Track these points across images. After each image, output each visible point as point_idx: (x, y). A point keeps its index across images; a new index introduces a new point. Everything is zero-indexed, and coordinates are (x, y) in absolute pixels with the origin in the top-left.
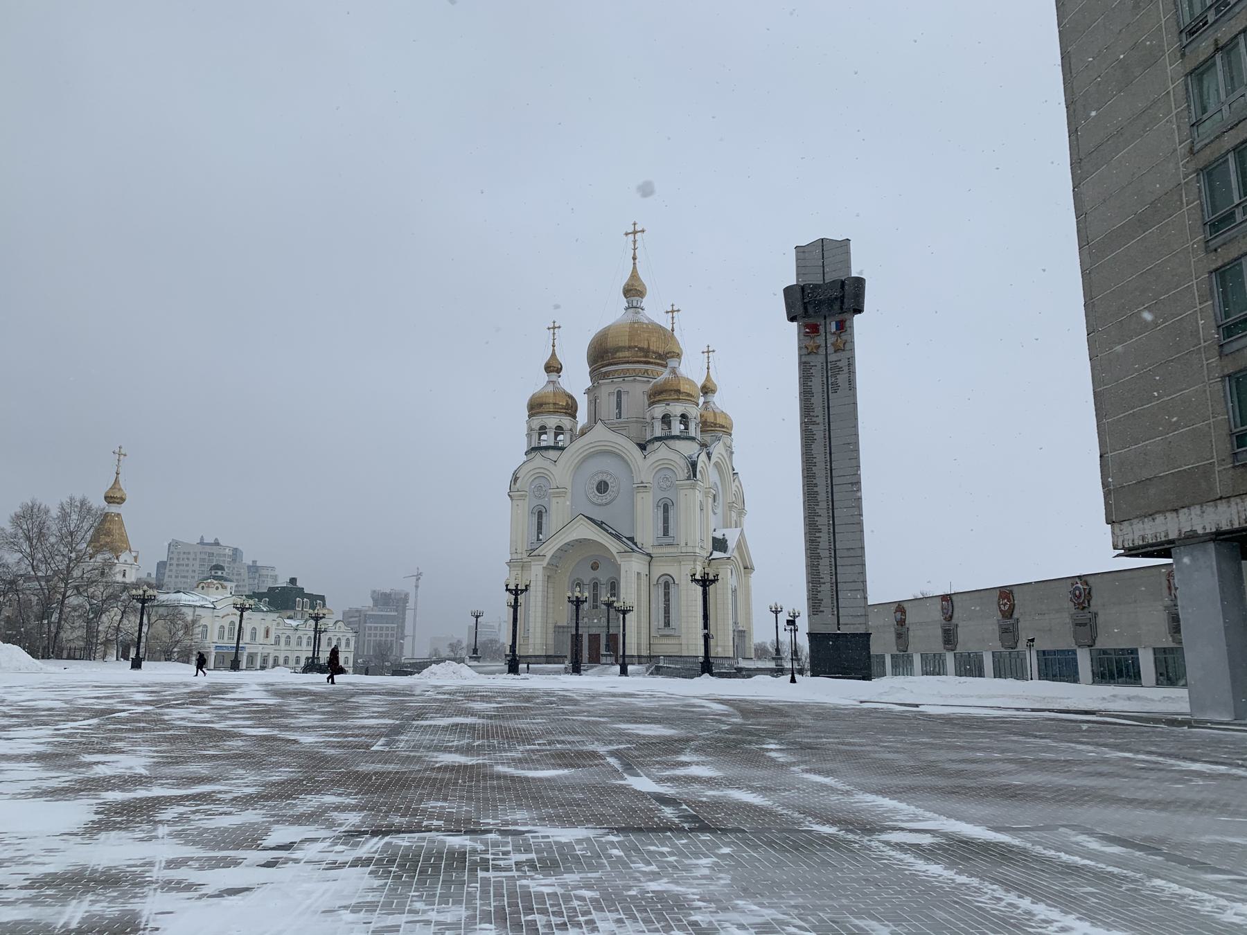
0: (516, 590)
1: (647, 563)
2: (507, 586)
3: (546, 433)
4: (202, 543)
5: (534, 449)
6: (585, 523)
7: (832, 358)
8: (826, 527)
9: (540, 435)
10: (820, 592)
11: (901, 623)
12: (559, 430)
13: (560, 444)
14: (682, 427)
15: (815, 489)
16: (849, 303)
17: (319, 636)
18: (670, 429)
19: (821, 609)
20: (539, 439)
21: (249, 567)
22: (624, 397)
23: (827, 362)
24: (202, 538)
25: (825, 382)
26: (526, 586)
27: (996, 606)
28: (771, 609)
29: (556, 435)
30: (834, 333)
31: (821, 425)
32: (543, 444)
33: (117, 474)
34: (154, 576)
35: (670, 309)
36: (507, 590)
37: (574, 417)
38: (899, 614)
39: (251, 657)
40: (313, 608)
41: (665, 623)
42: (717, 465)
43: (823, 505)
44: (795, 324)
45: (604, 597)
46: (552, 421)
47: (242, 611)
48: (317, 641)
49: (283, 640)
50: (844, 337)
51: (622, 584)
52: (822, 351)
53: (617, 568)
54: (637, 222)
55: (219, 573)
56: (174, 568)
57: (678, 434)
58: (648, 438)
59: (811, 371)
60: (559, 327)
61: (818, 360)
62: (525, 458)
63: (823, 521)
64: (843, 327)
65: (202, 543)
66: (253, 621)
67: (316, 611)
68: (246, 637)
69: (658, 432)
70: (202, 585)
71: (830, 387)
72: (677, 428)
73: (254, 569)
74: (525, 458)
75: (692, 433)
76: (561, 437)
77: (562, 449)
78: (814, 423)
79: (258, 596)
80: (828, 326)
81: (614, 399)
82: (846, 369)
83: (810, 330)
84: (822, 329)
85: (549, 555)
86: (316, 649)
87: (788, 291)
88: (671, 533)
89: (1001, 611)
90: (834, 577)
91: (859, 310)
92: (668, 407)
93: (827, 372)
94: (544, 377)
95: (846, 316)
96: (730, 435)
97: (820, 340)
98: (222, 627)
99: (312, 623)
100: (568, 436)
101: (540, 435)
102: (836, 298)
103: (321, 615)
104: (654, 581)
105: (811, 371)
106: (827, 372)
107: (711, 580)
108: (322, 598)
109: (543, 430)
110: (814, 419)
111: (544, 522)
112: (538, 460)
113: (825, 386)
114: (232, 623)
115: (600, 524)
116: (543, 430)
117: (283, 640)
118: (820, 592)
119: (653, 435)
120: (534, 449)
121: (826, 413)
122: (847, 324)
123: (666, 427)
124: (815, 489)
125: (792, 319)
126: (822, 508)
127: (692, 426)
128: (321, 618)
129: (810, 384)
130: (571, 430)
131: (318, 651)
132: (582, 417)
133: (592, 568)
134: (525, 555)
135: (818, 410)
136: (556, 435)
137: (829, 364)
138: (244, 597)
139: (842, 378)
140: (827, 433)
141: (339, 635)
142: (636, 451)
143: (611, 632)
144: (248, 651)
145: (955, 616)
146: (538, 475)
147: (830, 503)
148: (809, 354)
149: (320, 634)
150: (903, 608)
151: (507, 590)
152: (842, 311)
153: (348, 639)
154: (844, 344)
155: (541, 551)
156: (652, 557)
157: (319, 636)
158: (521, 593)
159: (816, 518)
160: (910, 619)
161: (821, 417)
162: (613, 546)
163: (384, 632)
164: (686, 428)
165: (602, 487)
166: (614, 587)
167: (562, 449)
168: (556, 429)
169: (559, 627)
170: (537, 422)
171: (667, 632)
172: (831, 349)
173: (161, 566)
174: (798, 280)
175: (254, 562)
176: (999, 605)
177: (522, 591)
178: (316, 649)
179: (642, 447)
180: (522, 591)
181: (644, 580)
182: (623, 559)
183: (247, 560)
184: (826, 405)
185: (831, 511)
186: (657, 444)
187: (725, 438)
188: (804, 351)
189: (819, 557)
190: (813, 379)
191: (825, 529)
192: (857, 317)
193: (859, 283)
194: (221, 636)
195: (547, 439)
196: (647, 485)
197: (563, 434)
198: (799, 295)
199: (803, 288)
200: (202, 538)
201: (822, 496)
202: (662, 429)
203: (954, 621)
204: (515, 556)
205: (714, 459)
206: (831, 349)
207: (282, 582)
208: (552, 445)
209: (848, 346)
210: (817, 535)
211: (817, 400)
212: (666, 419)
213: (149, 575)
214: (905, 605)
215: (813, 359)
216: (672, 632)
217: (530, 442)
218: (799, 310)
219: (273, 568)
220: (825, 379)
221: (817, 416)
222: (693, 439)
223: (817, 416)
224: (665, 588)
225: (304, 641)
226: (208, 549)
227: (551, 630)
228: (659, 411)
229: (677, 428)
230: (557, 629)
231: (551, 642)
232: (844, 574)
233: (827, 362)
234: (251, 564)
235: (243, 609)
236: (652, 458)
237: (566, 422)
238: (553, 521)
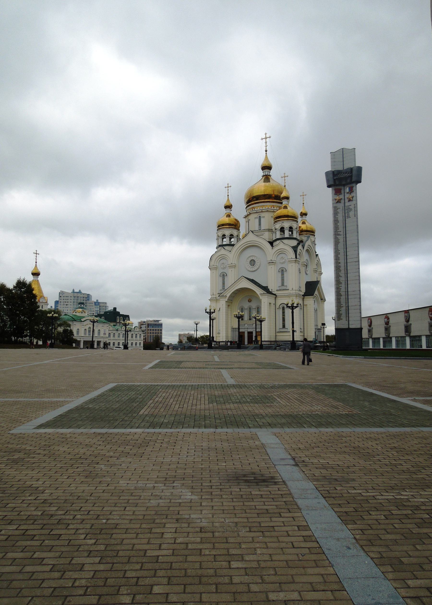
0: (210, 312)
1: (274, 299)
2: (206, 310)
3: (225, 238)
4: (73, 292)
5: (220, 246)
6: (244, 280)
7: (347, 204)
8: (344, 282)
9: (223, 239)
10: (341, 310)
11: (387, 323)
12: (231, 236)
13: (233, 243)
14: (291, 233)
15: (339, 265)
16: (354, 179)
17: (127, 333)
18: (284, 234)
19: (341, 318)
20: (223, 241)
21: (95, 303)
22: (262, 220)
23: (345, 206)
24: (73, 290)
25: (344, 215)
26: (214, 310)
27: (427, 315)
28: (333, 318)
29: (230, 239)
30: (348, 193)
31: (342, 235)
32: (224, 243)
33: (36, 262)
34: (53, 307)
35: (283, 176)
36: (206, 312)
37: (239, 230)
38: (386, 320)
39: (99, 343)
40: (124, 320)
41: (283, 326)
42: (307, 250)
43: (343, 272)
44: (331, 189)
45: (254, 314)
46: (227, 232)
47: (94, 323)
48: (126, 335)
49: (112, 335)
50: (353, 194)
51: (262, 309)
52: (342, 201)
53: (260, 301)
54: (267, 133)
55: (82, 306)
56: (62, 303)
57: (288, 236)
58: (274, 239)
59: (338, 211)
60: (231, 187)
61: (341, 205)
62: (216, 250)
63: (342, 279)
64: (351, 190)
65: (73, 292)
66: (98, 327)
67: (125, 322)
68: (96, 334)
69: (278, 236)
70: (75, 311)
71: (346, 217)
72: (287, 234)
73: (97, 303)
74: (216, 250)
75: (295, 235)
76: (232, 240)
77: (233, 245)
78: (339, 235)
79: (99, 316)
80: (345, 190)
81: (257, 220)
82: (353, 209)
83: (337, 192)
84: (342, 191)
85: (228, 296)
86: (126, 339)
87: (327, 174)
88: (285, 284)
89: (430, 317)
90: (347, 304)
91: (360, 182)
92: (283, 224)
93: (345, 211)
94: (224, 211)
95: (354, 185)
96: (314, 235)
97: (342, 196)
98: (85, 330)
99: (124, 327)
100: (236, 239)
101: (223, 239)
102: (349, 177)
103: (127, 324)
104: (277, 306)
105: (338, 211)
106: (345, 211)
107: (295, 307)
108: (128, 316)
109: (224, 236)
110: (339, 233)
111: (225, 280)
112: (223, 251)
113: (344, 217)
114: (90, 328)
115: (253, 281)
116: (224, 236)
117: (112, 335)
118: (341, 310)
119: (276, 237)
120: (220, 246)
121: (345, 230)
122: (354, 188)
123: (283, 233)
124: (339, 265)
125: (329, 186)
126: (342, 273)
127: (295, 232)
128: (128, 325)
129: (337, 216)
130: (237, 236)
131: (127, 340)
132: (243, 230)
133: (248, 301)
134: (217, 296)
135: (341, 229)
136: (230, 239)
137: (346, 207)
138: (94, 317)
139: (351, 214)
140: (345, 239)
141: (136, 333)
142: (269, 245)
143: (241, 330)
144: (97, 340)
145: (411, 319)
146: (222, 258)
147: (346, 271)
148: (337, 203)
149: (127, 332)
150: (388, 317)
151: (206, 312)
152: (352, 182)
153: (140, 335)
154: (352, 198)
155: (224, 294)
156: (276, 296)
157: (127, 333)
158: (212, 313)
159: (340, 278)
160: (391, 322)
161: (342, 232)
162: (259, 291)
163: (157, 332)
164: (292, 234)
165: (253, 262)
166: (258, 310)
167: (233, 245)
168: (230, 236)
169: (234, 329)
170: (221, 233)
171: (284, 330)
172: (347, 200)
173: (57, 302)
174: (332, 168)
175: (97, 300)
176: (429, 314)
177: (213, 312)
178: (126, 339)
179: (271, 243)
180: (213, 312)
181: (273, 306)
182: (262, 297)
183: (94, 299)
184: (344, 226)
185: (346, 275)
186: (278, 242)
187: (312, 238)
188: (335, 202)
189: (341, 295)
190: (339, 214)
191: (343, 283)
192: (359, 185)
193: (359, 169)
194: (85, 333)
195: (226, 241)
196: (274, 261)
197: (233, 238)
198: (331, 176)
199: (333, 172)
200: (73, 290)
201: (342, 268)
202: (281, 234)
203: (410, 323)
204: (213, 296)
205: (306, 248)
206: (347, 200)
207: (110, 308)
208: (229, 243)
209: (354, 198)
210: (340, 285)
211: (340, 225)
212: (282, 230)
213: (52, 307)
214: (388, 315)
215: (339, 205)
216: (286, 330)
217: (218, 243)
218: (332, 183)
219: (106, 303)
220: (344, 214)
221: (341, 232)
222: (295, 239)
223: (341, 232)
224: (283, 310)
225: (121, 335)
226: (76, 295)
227: (230, 330)
228: (278, 226)
229: (287, 234)
230: (233, 330)
231: (230, 335)
232: (352, 302)
233: (345, 206)
234: (96, 301)
235: (94, 322)
236: (276, 249)
237: (235, 232)
238: (229, 281)
